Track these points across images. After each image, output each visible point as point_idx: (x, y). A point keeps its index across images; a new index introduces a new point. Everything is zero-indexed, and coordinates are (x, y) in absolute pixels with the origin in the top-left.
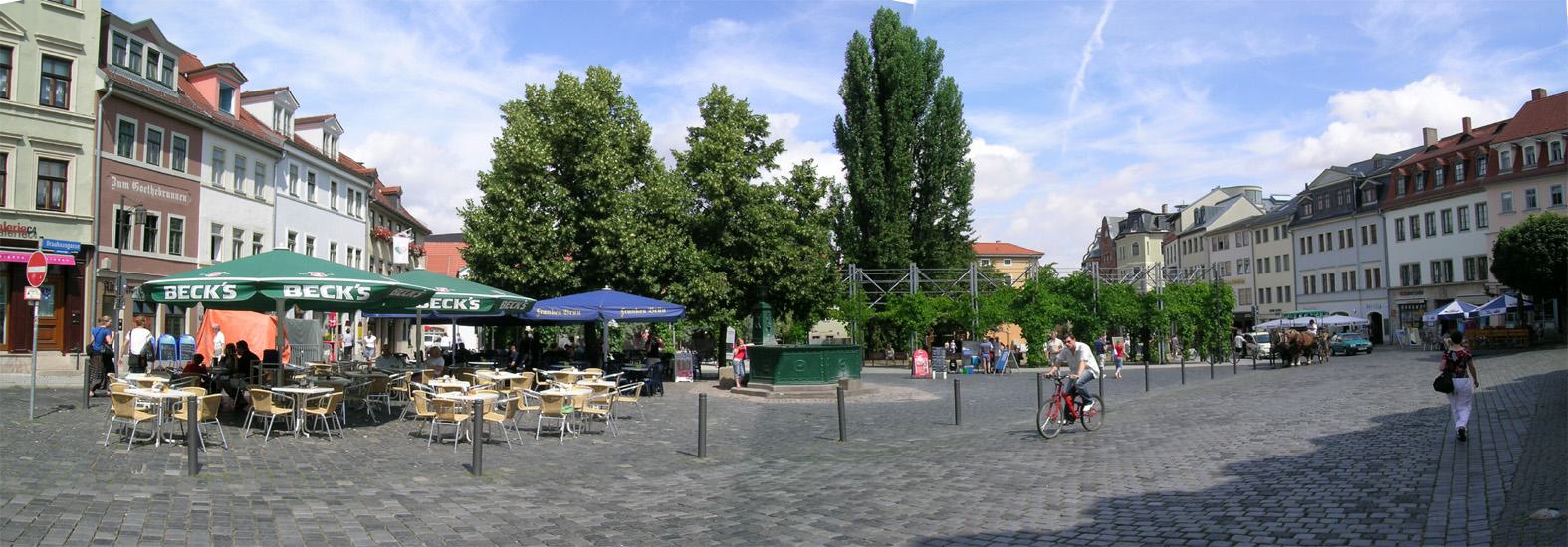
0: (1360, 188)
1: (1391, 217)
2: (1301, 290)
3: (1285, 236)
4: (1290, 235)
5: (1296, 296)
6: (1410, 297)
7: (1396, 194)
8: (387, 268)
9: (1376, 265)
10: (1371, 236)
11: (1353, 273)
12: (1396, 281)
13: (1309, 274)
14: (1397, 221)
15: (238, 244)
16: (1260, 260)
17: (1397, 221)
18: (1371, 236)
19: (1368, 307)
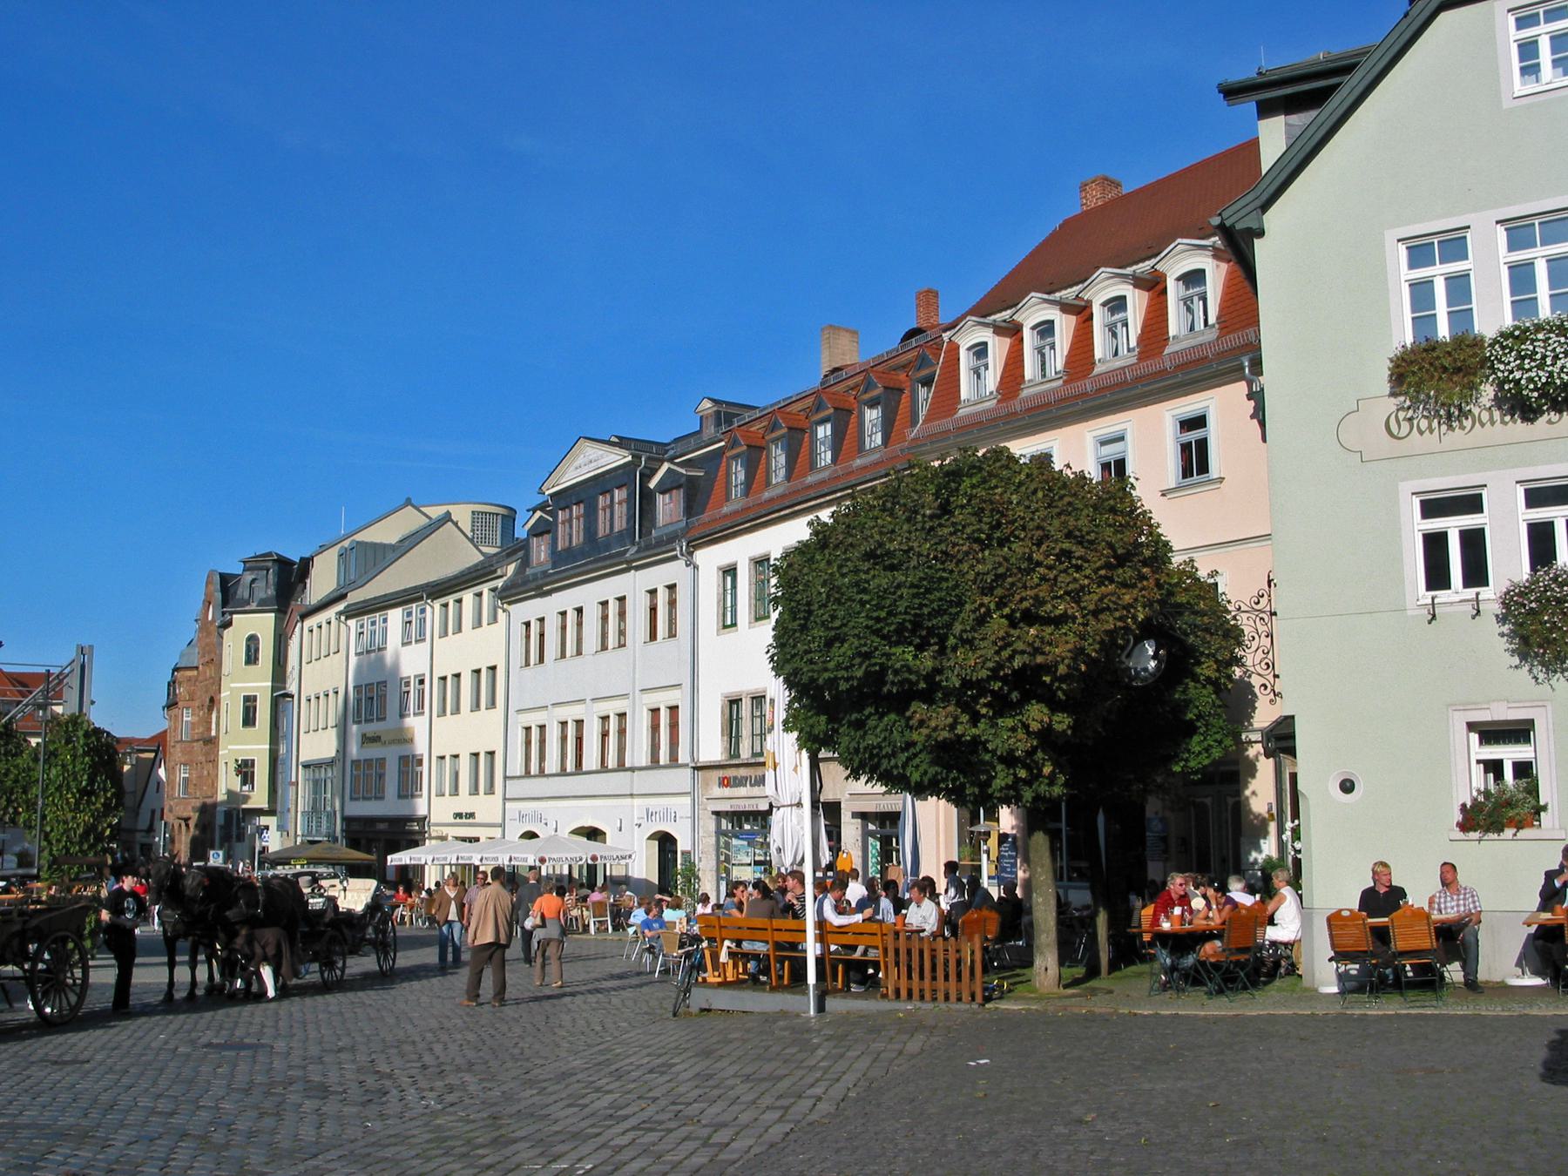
0: (652, 485)
1: (711, 558)
2: (517, 768)
3: (494, 619)
4: (501, 615)
5: (506, 778)
6: (742, 791)
7: (727, 498)
8: (613, 921)
9: (672, 697)
10: (663, 617)
11: (542, 727)
12: (712, 748)
13: (534, 719)
14: (384, 719)
15: (934, 991)
16: (444, 679)
17: (384, 719)
18: (663, 617)
19: (650, 815)
